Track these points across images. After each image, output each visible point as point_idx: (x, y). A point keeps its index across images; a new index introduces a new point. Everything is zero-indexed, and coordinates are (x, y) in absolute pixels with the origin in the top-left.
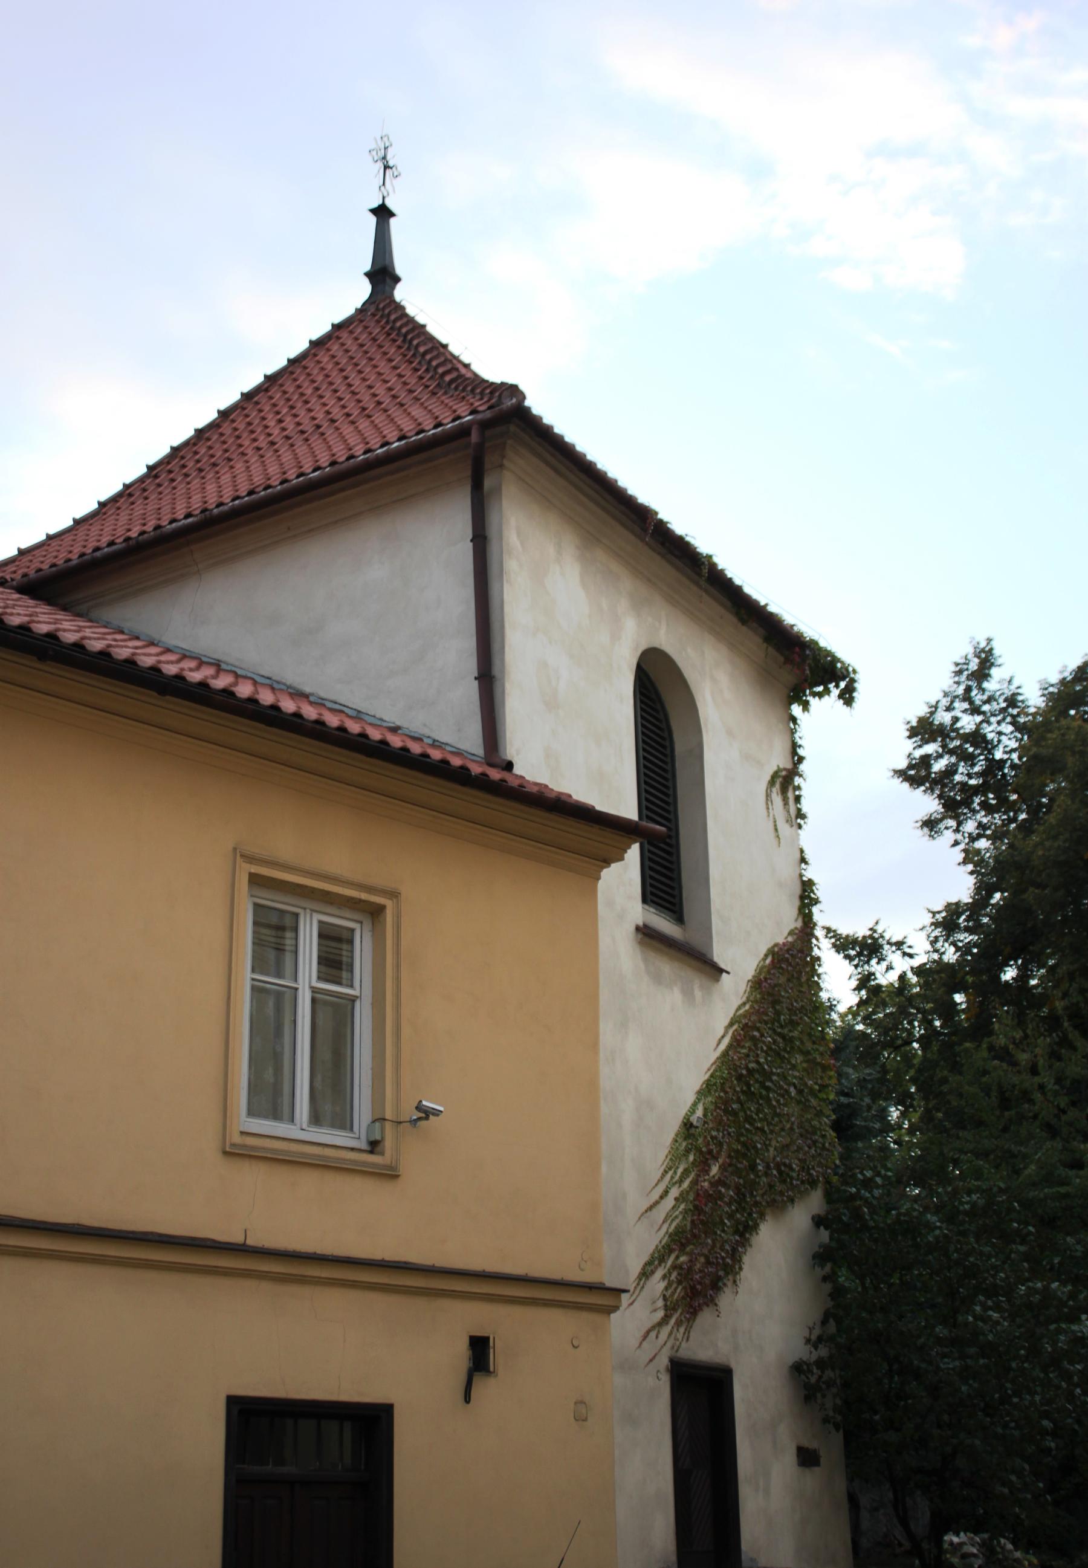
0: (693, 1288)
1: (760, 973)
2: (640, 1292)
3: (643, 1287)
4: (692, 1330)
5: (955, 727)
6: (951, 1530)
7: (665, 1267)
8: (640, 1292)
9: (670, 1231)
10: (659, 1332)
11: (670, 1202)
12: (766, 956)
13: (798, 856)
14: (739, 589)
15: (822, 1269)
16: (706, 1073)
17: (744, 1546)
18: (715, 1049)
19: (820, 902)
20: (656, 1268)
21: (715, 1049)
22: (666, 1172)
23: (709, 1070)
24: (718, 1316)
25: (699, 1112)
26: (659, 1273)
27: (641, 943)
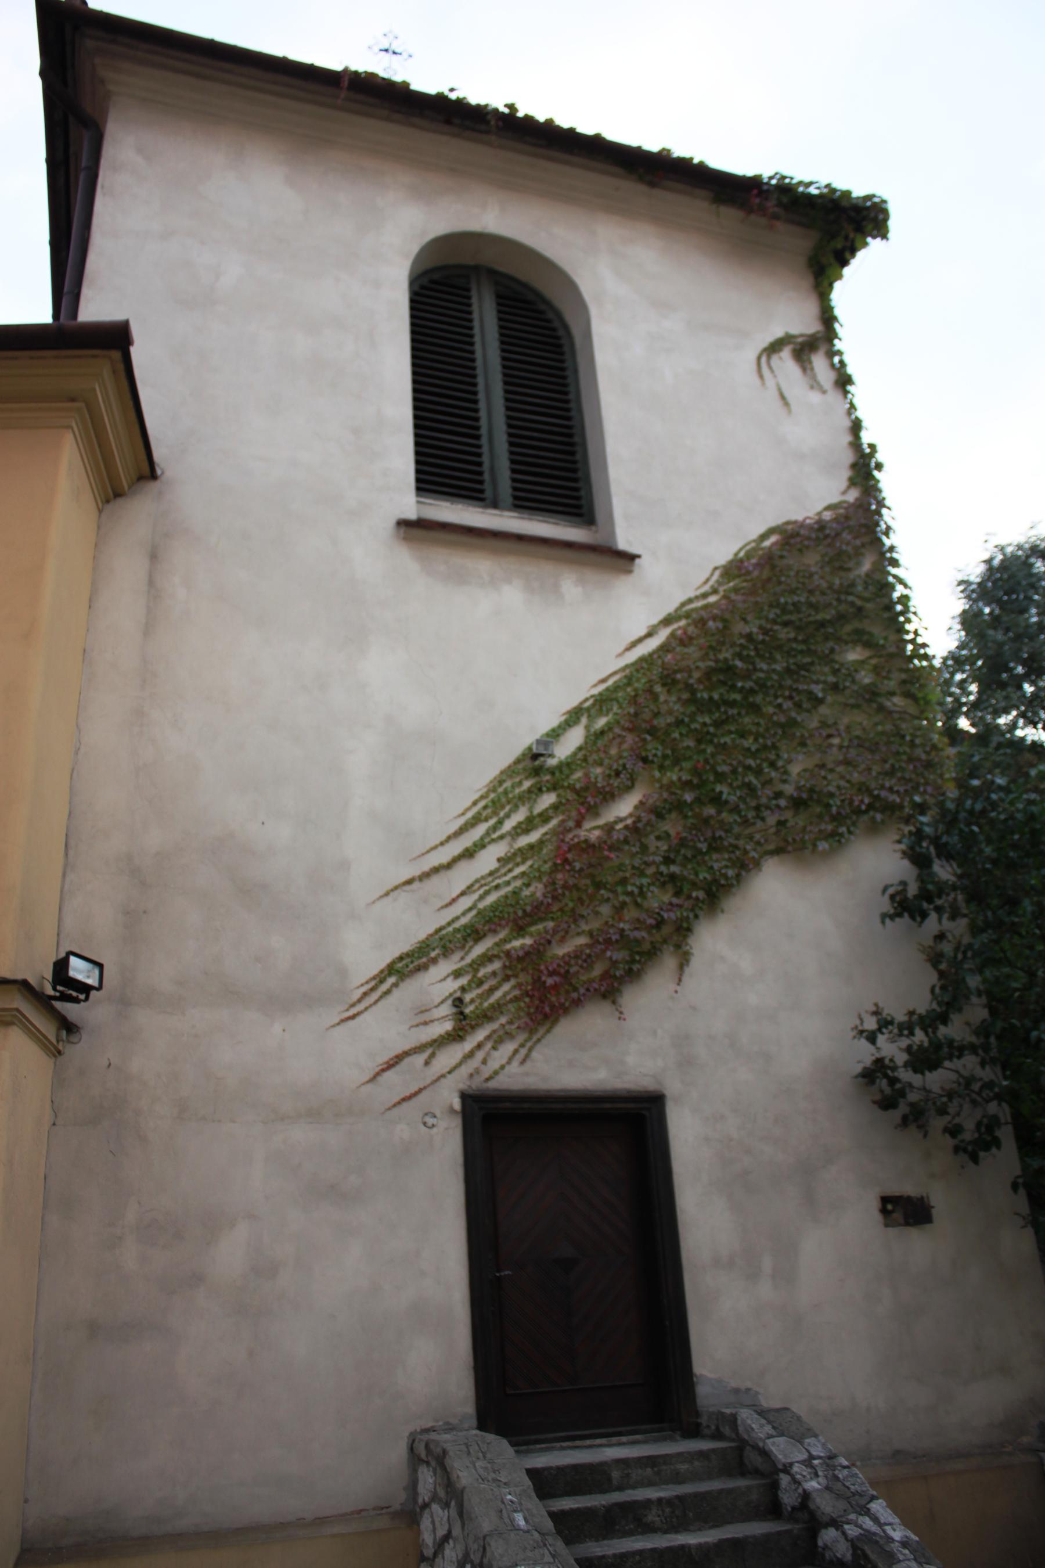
0: (538, 982)
1: (749, 555)
2: (381, 997)
3: (388, 992)
4: (539, 1047)
5: (53, 1002)
6: (1024, 659)
7: (462, 958)
8: (381, 997)
9: (481, 905)
10: (433, 1055)
11: (487, 860)
12: (771, 531)
13: (384, 53)
14: (702, 166)
15: (934, 804)
16: (595, 686)
17: (702, 1391)
18: (620, 655)
19: (887, 239)
20: (434, 961)
21: (620, 655)
22: (476, 820)
23: (603, 681)
24: (620, 1018)
25: (574, 739)
26: (445, 967)
27: (406, 539)
